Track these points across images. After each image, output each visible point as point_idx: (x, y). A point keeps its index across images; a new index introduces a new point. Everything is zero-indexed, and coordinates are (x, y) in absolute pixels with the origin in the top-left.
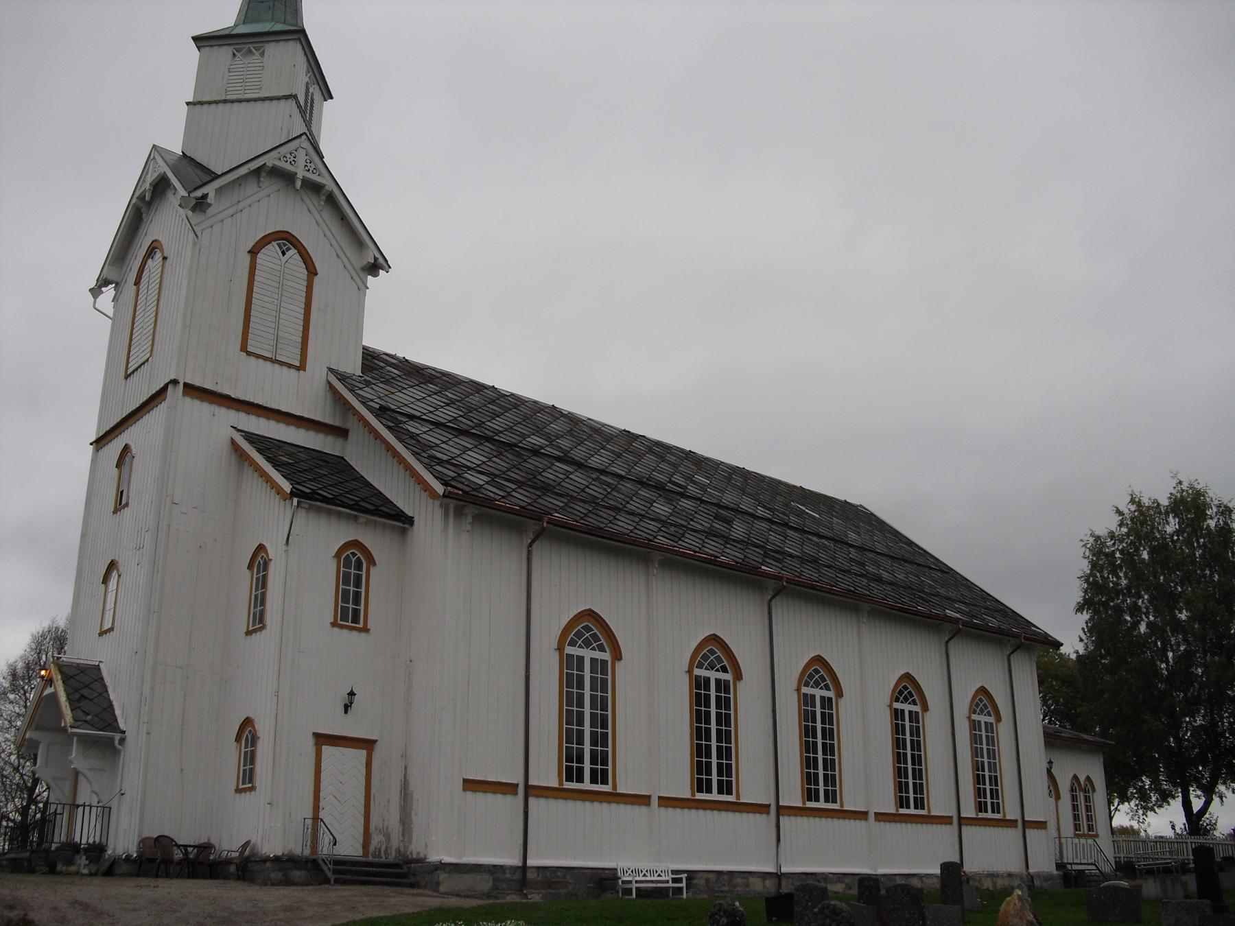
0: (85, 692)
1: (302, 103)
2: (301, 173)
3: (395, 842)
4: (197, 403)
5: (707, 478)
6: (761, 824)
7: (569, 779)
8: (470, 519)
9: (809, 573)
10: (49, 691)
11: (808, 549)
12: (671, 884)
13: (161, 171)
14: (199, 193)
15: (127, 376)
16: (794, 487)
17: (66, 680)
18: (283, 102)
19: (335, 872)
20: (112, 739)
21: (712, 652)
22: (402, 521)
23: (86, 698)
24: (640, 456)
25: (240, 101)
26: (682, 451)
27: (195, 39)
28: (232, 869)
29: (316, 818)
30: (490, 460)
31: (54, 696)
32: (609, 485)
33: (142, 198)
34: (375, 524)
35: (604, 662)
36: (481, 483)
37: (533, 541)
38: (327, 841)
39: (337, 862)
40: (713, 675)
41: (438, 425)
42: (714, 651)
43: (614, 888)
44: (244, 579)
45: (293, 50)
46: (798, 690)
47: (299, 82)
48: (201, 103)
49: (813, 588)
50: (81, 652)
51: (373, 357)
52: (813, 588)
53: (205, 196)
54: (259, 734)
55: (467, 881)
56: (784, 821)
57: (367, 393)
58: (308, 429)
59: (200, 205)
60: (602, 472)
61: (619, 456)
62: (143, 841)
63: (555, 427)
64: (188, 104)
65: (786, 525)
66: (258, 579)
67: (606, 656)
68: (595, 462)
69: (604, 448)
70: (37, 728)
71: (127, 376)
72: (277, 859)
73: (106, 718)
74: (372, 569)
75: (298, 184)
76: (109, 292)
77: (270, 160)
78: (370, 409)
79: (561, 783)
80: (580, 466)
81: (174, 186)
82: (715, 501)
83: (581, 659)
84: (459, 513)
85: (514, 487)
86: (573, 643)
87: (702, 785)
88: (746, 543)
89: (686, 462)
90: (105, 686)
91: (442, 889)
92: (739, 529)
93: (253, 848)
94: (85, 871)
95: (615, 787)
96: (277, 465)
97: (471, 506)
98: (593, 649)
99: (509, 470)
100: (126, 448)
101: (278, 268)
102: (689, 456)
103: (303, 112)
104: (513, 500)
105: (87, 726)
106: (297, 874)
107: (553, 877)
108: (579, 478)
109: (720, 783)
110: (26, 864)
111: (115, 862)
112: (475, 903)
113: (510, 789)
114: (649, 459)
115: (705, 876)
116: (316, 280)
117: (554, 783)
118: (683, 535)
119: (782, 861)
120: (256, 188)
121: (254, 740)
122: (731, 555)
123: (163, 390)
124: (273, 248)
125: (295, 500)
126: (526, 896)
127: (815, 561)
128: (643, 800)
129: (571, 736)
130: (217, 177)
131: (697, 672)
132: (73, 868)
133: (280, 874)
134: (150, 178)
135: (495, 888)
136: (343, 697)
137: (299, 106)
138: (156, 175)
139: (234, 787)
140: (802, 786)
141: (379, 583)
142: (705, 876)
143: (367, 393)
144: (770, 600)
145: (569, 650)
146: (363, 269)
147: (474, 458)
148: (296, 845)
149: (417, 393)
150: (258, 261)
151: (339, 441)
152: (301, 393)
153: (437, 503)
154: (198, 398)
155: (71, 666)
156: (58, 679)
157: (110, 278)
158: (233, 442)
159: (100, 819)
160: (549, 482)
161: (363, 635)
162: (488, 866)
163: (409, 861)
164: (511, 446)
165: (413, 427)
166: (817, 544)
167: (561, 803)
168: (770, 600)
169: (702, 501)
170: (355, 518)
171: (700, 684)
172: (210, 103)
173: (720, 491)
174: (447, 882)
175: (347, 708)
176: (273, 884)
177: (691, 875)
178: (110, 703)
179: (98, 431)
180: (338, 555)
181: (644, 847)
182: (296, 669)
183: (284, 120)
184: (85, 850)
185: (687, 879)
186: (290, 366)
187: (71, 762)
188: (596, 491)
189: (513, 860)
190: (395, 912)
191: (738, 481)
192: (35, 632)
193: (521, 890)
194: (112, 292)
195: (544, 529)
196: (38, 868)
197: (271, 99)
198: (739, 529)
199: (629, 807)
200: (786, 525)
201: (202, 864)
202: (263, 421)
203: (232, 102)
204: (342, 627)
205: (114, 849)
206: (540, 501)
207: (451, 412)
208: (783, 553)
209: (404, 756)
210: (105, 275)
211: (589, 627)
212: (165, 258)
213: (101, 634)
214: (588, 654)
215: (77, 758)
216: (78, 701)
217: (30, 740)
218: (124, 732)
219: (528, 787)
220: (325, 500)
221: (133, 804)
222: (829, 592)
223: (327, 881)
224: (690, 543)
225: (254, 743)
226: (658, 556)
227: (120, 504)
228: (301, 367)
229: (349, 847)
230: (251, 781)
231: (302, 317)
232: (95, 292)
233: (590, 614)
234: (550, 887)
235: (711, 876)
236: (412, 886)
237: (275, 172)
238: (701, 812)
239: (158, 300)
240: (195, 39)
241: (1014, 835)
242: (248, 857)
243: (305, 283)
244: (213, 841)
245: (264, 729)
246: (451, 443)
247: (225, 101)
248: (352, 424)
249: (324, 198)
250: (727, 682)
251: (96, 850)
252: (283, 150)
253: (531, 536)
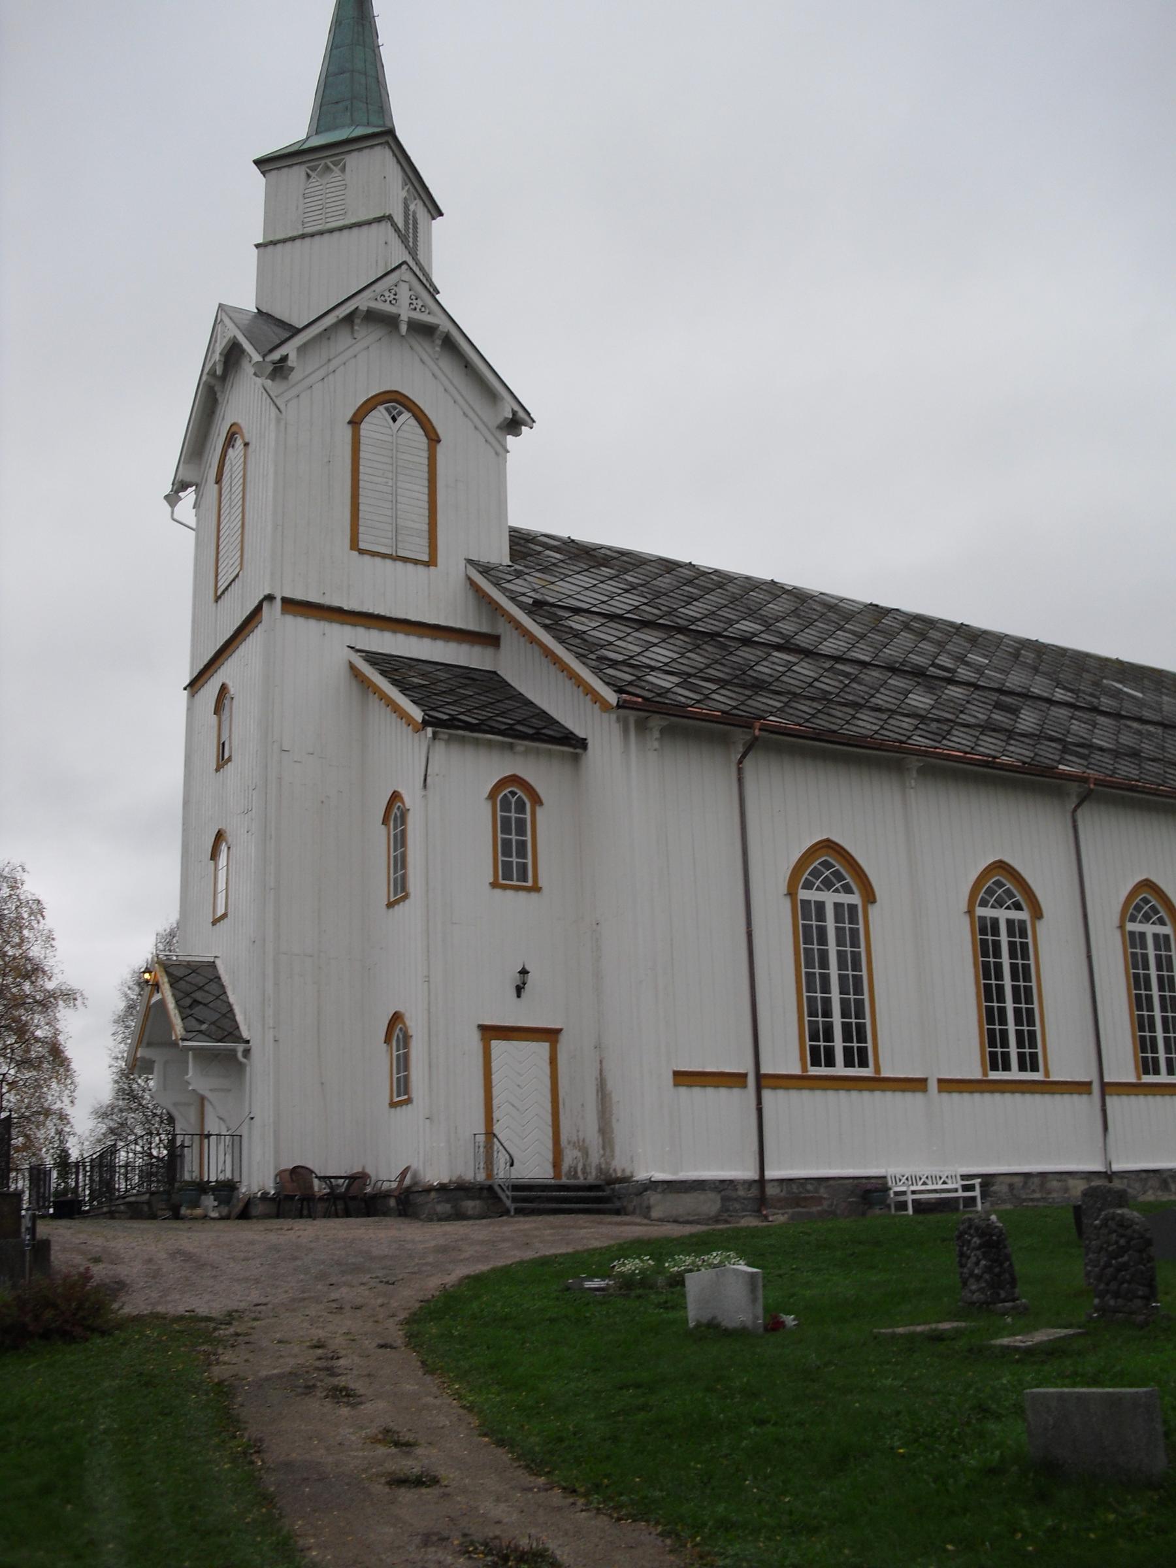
0: (198, 995)
1: (401, 225)
2: (405, 314)
3: (595, 1158)
4: (301, 621)
5: (985, 656)
6: (1084, 1106)
7: (816, 1062)
8: (656, 734)
9: (1126, 770)
10: (156, 997)
11: (1127, 739)
12: (960, 1194)
13: (230, 335)
14: (276, 356)
15: (218, 599)
16: (1107, 660)
17: (174, 982)
18: (374, 226)
19: (515, 1200)
20: (234, 1051)
21: (999, 884)
22: (572, 744)
23: (200, 1003)
24: (891, 635)
25: (321, 233)
26: (952, 624)
27: (258, 163)
28: (392, 1202)
29: (490, 1134)
30: (682, 655)
31: (162, 1003)
32: (847, 675)
33: (212, 373)
34: (538, 752)
35: (853, 908)
36: (669, 685)
37: (744, 756)
38: (502, 1161)
39: (516, 1188)
40: (1003, 915)
41: (612, 617)
42: (1002, 883)
43: (883, 1203)
44: (379, 836)
45: (382, 157)
46: (1122, 927)
47: (394, 197)
48: (274, 243)
49: (1132, 789)
50: (196, 950)
51: (528, 541)
52: (1132, 789)
53: (284, 359)
54: (411, 1032)
55: (686, 1203)
56: (1113, 1102)
57: (518, 586)
58: (447, 640)
59: (280, 370)
60: (837, 659)
61: (862, 637)
62: (279, 1174)
63: (774, 608)
64: (257, 246)
65: (1095, 710)
66: (395, 836)
67: (855, 899)
68: (828, 647)
69: (841, 628)
70: (149, 1045)
71: (218, 599)
72: (443, 1188)
73: (225, 1026)
74: (539, 810)
75: (404, 328)
76: (188, 497)
77: (363, 303)
78: (521, 605)
79: (804, 1069)
80: (807, 653)
81: (249, 353)
82: (996, 686)
83: (820, 906)
84: (642, 727)
85: (714, 687)
86: (808, 885)
87: (997, 1061)
88: (1038, 737)
89: (956, 639)
90: (223, 986)
91: (655, 1214)
92: (1028, 720)
93: (415, 1176)
94: (214, 1214)
95: (877, 1069)
96: (404, 689)
97: (658, 716)
98: (837, 891)
99: (708, 666)
100: (223, 688)
101: (389, 439)
102: (961, 630)
103: (404, 239)
104: (711, 703)
105: (201, 1036)
106: (470, 1205)
107: (800, 1192)
108: (806, 669)
109: (1021, 1056)
110: (146, 1208)
111: (249, 1203)
112: (687, 1230)
113: (735, 1080)
114: (905, 639)
115: (1008, 1180)
116: (441, 449)
117: (796, 1070)
118: (949, 732)
119: (1112, 1156)
120: (350, 341)
121: (406, 1039)
122: (1015, 754)
123: (258, 609)
124: (380, 415)
125: (429, 730)
126: (766, 1217)
127: (1135, 754)
128: (917, 1085)
129: (814, 1010)
130: (298, 331)
131: (981, 911)
132: (198, 1212)
133: (448, 1207)
134: (219, 348)
135: (724, 1209)
136: (513, 978)
137: (397, 230)
138: (225, 341)
139: (387, 1101)
140: (1135, 1055)
141: (549, 828)
142: (1008, 1180)
143: (518, 586)
144: (1075, 811)
145: (804, 894)
146: (499, 427)
147: (662, 654)
148: (470, 1171)
149: (585, 580)
150: (362, 433)
151: (489, 652)
152: (436, 595)
153: (614, 717)
154: (302, 616)
155: (179, 965)
156: (164, 981)
157: (188, 479)
158: (352, 667)
159: (229, 1150)
160: (760, 678)
161: (534, 895)
162: (714, 1182)
163: (611, 1181)
164: (713, 636)
165: (578, 623)
166: (1139, 732)
168: (1075, 811)
169: (977, 687)
170: (511, 747)
171: (986, 928)
172: (284, 241)
173: (1002, 671)
174: (660, 1206)
175: (519, 990)
176: (440, 1220)
177: (988, 1180)
178: (230, 1005)
179: (191, 673)
180: (492, 796)
181: (922, 1147)
182: (455, 944)
183: (375, 250)
184: (214, 1189)
185: (982, 1185)
186: (416, 562)
187: (188, 1083)
188: (829, 684)
189: (751, 1174)
190: (580, 1248)
191: (1028, 656)
192: (160, 930)
193: (759, 1211)
194: (193, 496)
195: (756, 738)
196: (160, 1213)
197: (359, 225)
198: (1028, 720)
199: (898, 1095)
200: (1095, 710)
201: (355, 1199)
202: (387, 635)
203: (312, 235)
204: (505, 887)
205: (249, 1186)
206: (750, 702)
207: (633, 600)
208: (1090, 746)
209: (598, 1047)
210: (180, 477)
211: (829, 863)
212: (246, 444)
213: (214, 923)
214: (830, 898)
215: (197, 1079)
216: (190, 1007)
217: (143, 1059)
218: (248, 1042)
219: (760, 1078)
221: (267, 1131)
222: (1156, 793)
223: (506, 1212)
224: (960, 740)
225: (406, 1045)
226: (914, 762)
227: (223, 761)
228: (431, 562)
229: (533, 1165)
230: (406, 1092)
231: (426, 498)
232: (172, 499)
233: (828, 845)
234: (798, 1205)
235: (1016, 1179)
236: (617, 1212)
237: (373, 317)
238: (997, 1096)
239: (244, 498)
240: (258, 163)
242: (408, 1188)
243: (426, 454)
244: (369, 1171)
245: (415, 1024)
246: (629, 639)
247: (303, 236)
248: (503, 629)
249: (439, 342)
250: (1022, 923)
251: (227, 1189)
252: (378, 287)
253: (741, 750)
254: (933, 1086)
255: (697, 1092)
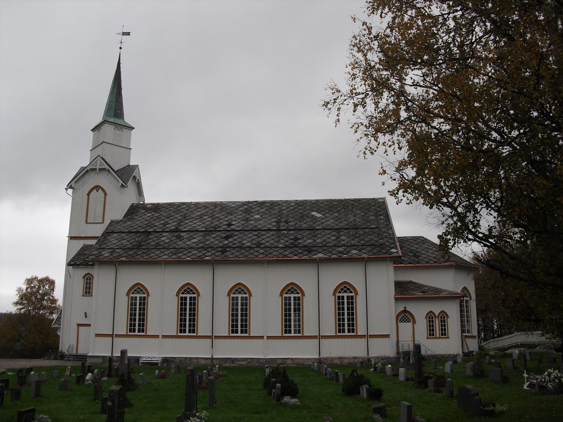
113: (217, 337)
116: (107, 196)
128: (157, 336)
167: (127, 338)
211: (138, 288)
220: (78, 265)
228: (103, 222)
237: (92, 170)
241: (364, 341)
254: (160, 337)
255: (101, 338)
